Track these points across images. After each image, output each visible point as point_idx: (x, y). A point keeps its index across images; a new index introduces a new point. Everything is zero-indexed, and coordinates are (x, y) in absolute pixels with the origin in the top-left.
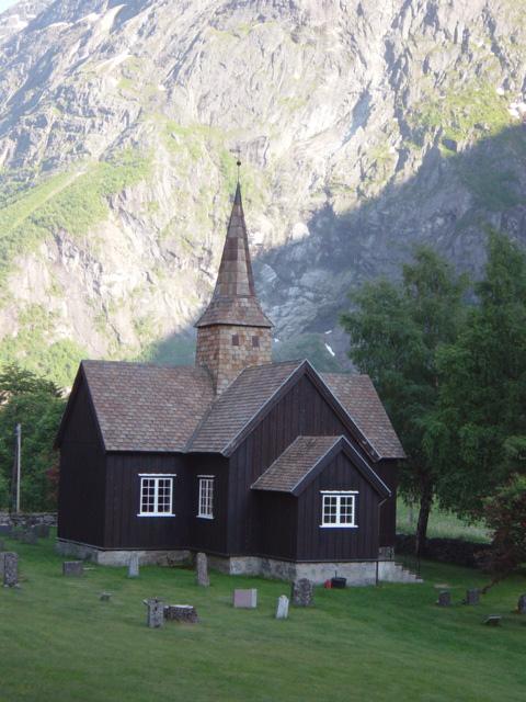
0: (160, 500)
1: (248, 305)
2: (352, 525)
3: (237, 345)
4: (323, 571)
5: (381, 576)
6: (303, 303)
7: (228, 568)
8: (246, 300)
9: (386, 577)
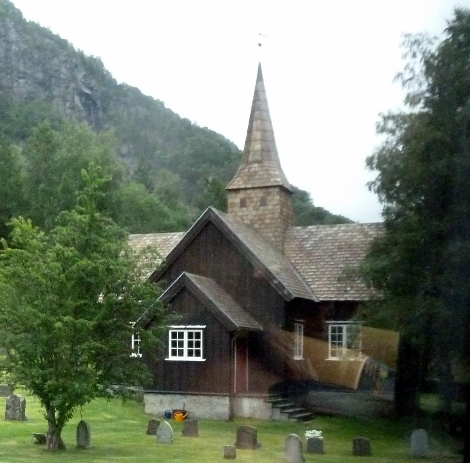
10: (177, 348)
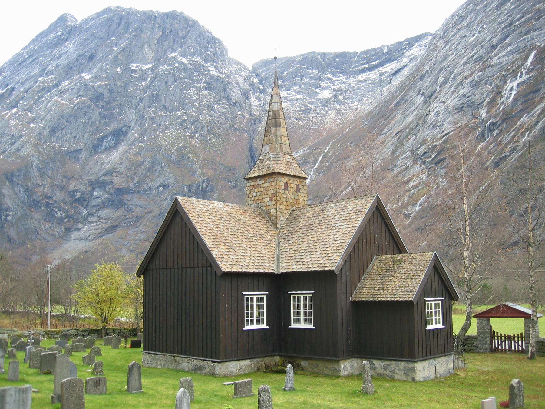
3: (287, 190)
6: (99, 224)
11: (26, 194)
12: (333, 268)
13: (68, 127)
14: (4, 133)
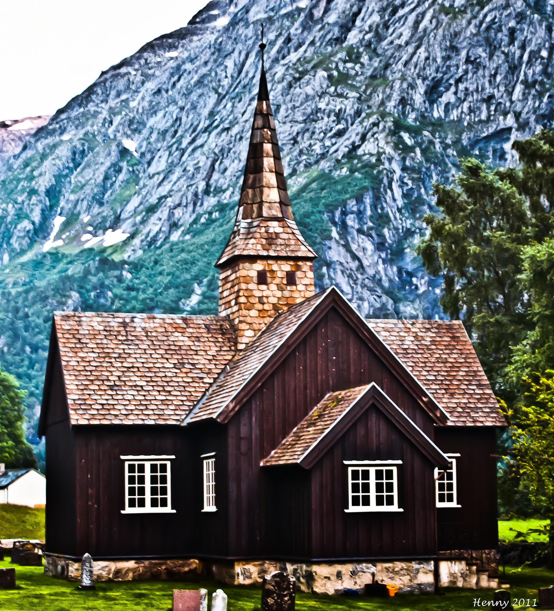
0: (154, 491)
1: (279, 230)
2: (168, 509)
4: (354, 574)
5: (445, 580)
7: (233, 577)
8: (275, 224)
9: (453, 582)
10: (361, 494)
11: (380, 257)
12: (214, 416)
13: (470, 75)
14: (318, 110)
